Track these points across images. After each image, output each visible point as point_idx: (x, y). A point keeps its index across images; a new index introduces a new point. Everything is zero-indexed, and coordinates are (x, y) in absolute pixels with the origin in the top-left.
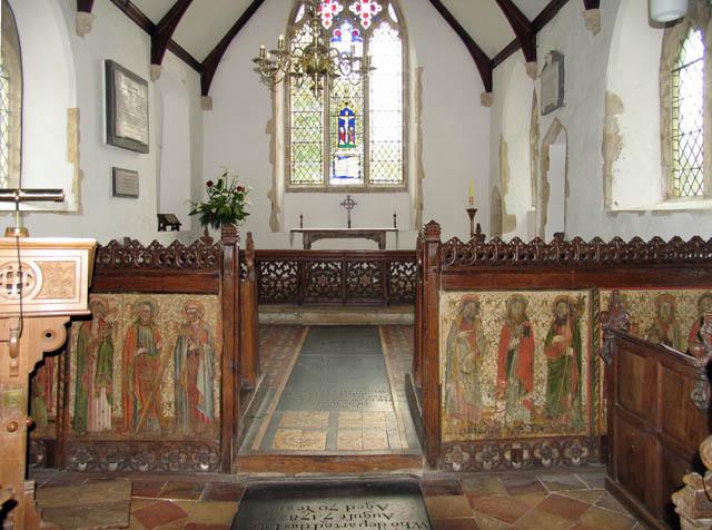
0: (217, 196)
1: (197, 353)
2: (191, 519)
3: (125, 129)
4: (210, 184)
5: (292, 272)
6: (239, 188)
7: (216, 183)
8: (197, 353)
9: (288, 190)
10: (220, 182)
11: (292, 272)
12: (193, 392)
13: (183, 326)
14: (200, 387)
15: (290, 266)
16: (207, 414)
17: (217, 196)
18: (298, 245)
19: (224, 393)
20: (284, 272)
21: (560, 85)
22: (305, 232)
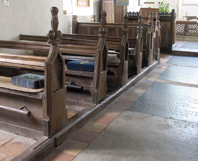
0: (161, 6)
1: (166, 32)
2: (173, 45)
3: (140, 4)
4: (159, 3)
5: (183, 27)
6: (168, 4)
7: (161, 3)
8: (166, 32)
9: (183, 5)
10: (162, 2)
11: (183, 27)
12: (165, 39)
13: (164, 27)
14: (166, 38)
15: (183, 25)
16: (167, 43)
17: (161, 6)
18: (185, 20)
19: (77, 155)
20: (181, 27)
21: (74, 75)
22: (188, 17)
